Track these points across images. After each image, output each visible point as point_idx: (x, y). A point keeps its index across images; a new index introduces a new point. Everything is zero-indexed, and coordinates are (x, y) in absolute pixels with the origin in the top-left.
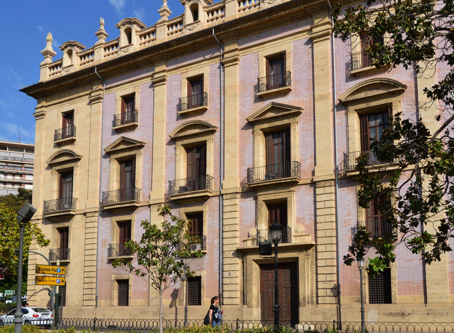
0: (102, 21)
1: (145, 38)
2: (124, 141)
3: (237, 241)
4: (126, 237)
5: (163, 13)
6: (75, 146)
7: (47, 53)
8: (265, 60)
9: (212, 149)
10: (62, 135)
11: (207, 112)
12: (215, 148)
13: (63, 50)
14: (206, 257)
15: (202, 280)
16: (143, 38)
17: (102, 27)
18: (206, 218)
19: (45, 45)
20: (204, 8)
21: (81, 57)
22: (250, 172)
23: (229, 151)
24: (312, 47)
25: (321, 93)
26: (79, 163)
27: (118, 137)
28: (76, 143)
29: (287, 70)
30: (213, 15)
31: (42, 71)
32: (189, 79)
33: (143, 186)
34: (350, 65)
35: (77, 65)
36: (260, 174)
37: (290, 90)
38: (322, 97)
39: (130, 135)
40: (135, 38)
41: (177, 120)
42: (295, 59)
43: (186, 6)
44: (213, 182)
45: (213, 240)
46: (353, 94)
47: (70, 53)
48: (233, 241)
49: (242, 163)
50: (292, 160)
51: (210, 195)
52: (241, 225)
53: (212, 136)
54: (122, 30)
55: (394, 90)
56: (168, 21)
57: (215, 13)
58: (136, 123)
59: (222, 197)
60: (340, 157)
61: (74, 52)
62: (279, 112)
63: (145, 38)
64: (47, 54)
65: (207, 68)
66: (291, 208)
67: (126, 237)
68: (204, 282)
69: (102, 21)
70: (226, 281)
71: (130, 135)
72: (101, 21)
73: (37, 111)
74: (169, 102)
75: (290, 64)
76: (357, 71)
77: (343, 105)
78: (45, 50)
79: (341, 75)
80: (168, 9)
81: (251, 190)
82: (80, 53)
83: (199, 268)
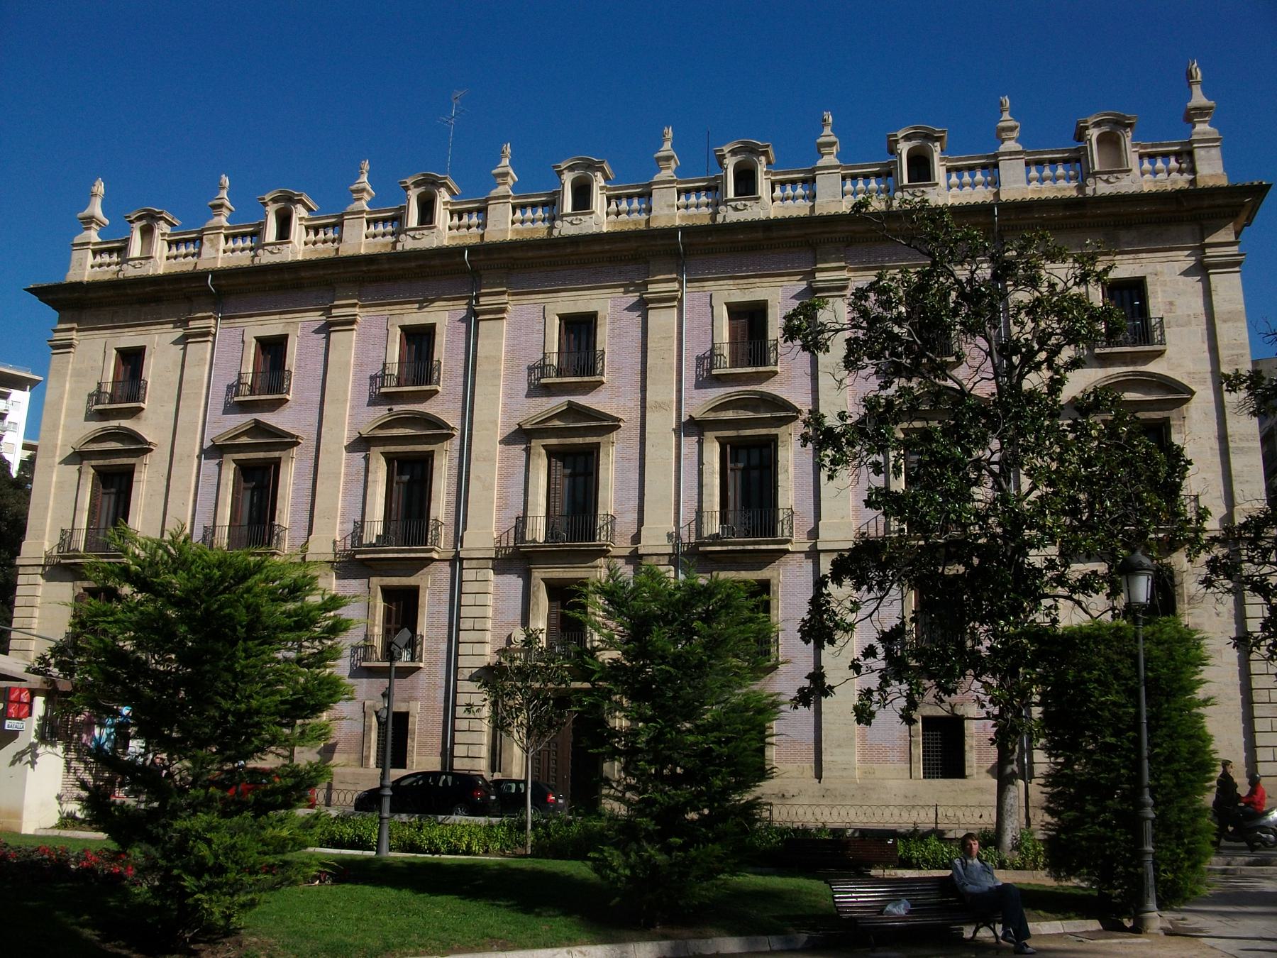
0: (226, 181)
1: (316, 233)
2: (259, 429)
3: (488, 649)
4: (393, 621)
5: (359, 195)
6: (142, 421)
7: (90, 220)
8: (557, 321)
9: (445, 470)
10: (111, 395)
11: (438, 396)
12: (450, 467)
13: (131, 222)
14: (422, 676)
15: (410, 719)
16: (312, 233)
17: (224, 194)
18: (425, 600)
19: (86, 204)
20: (445, 203)
21: (170, 243)
22: (360, 526)
23: (478, 478)
24: (185, 349)
25: (658, 399)
26: (147, 458)
27: (242, 420)
28: (143, 414)
29: (599, 347)
30: (460, 219)
31: (76, 255)
32: (404, 329)
33: (293, 524)
34: (234, 389)
35: (161, 258)
36: (538, 531)
37: (437, 392)
38: (660, 406)
39: (268, 418)
40: (297, 231)
41: (528, 396)
42: (613, 330)
43: (410, 192)
44: (443, 530)
45: (437, 644)
46: (714, 409)
47: (147, 232)
48: (478, 649)
49: (504, 504)
50: (780, 506)
51: (436, 556)
52: (494, 619)
53: (446, 444)
54: (413, 195)
55: (783, 414)
56: (515, 198)
57: (466, 217)
58: (142, 405)
59: (461, 565)
60: (688, 513)
61: (157, 232)
62: (580, 421)
63: (316, 233)
64: (92, 222)
65: (299, 329)
66: (537, 598)
67: (393, 621)
68: (415, 724)
69: (226, 181)
70: (461, 724)
71: (268, 418)
72: (222, 181)
73: (57, 336)
74: (360, 364)
75: (604, 337)
76: (241, 399)
77: (693, 427)
78: (87, 213)
79: (218, 402)
80: (369, 187)
81: (516, 559)
82: (307, 220)
83: (405, 696)
